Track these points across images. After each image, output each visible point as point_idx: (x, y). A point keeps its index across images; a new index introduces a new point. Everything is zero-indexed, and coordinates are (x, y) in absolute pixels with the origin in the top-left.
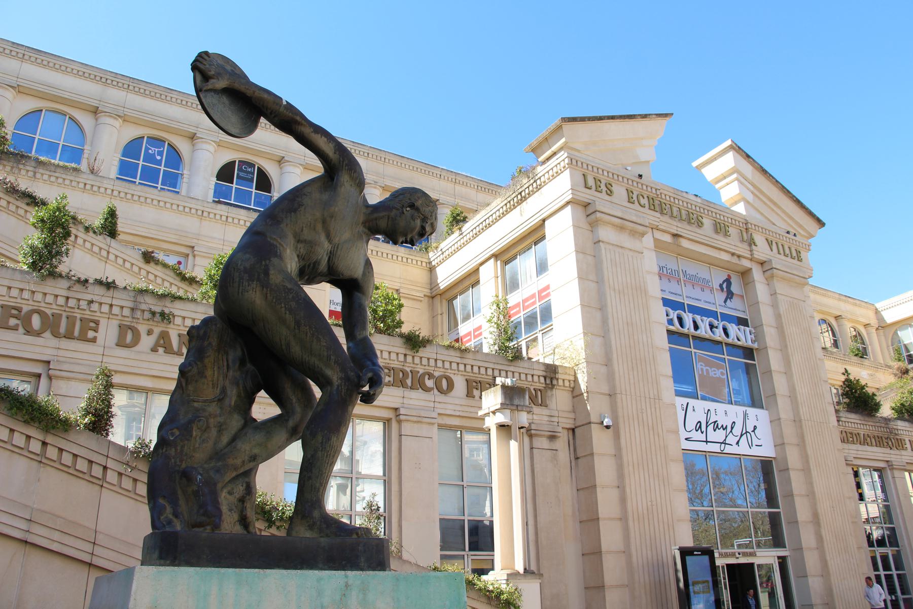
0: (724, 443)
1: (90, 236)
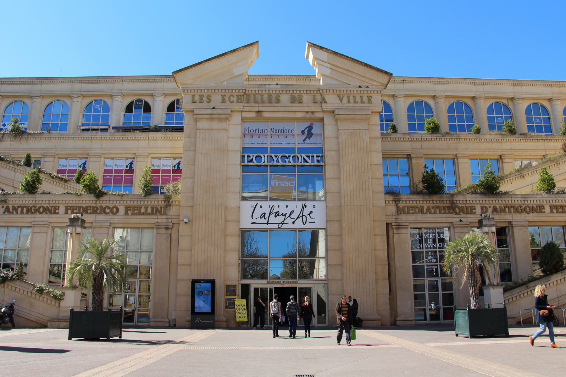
0: (282, 223)
1: (20, 167)
